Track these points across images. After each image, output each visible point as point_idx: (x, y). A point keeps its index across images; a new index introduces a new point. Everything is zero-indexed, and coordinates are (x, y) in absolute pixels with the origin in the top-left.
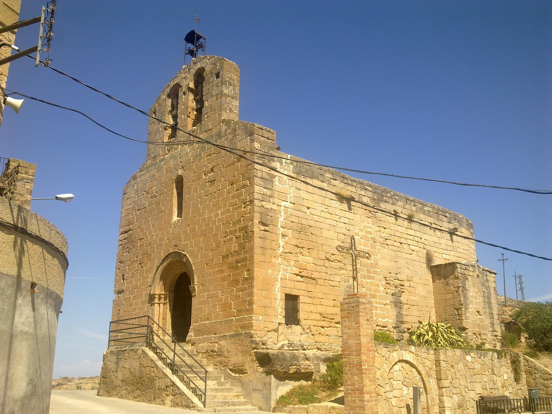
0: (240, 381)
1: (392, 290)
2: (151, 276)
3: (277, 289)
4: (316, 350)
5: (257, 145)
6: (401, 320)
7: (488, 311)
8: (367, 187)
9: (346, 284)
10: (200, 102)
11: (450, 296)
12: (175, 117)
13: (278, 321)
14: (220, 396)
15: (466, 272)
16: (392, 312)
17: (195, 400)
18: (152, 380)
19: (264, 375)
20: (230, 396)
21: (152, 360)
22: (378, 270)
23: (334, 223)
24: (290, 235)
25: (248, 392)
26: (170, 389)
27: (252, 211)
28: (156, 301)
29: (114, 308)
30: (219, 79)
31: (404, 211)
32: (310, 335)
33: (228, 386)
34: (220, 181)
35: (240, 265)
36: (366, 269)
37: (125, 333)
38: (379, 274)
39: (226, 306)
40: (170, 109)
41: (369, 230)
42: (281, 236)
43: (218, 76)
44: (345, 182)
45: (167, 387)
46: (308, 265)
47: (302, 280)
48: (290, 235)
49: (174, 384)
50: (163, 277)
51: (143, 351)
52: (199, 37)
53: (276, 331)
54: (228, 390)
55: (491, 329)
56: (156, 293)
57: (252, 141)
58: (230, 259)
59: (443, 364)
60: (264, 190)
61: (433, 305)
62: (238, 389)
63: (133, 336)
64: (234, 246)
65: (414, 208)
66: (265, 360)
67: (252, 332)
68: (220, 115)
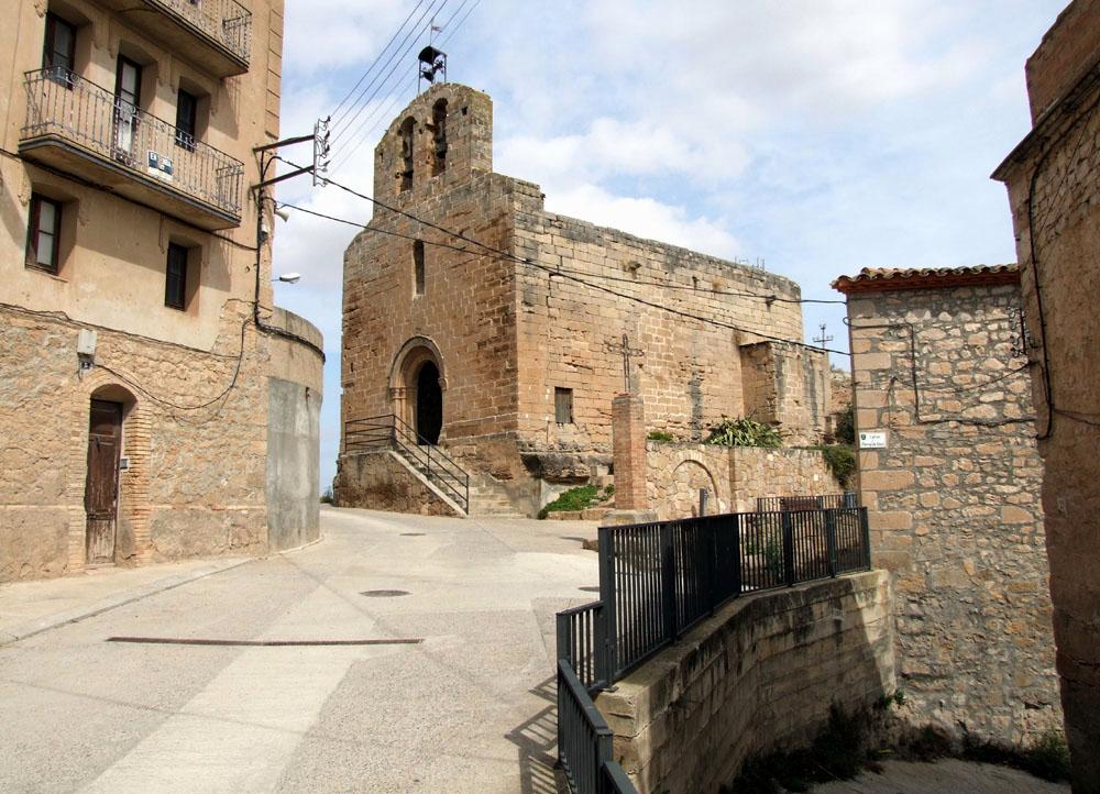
0: (504, 486)
1: (688, 377)
2: (389, 365)
5: (517, 205)
7: (809, 400)
10: (440, 140)
11: (762, 383)
12: (409, 160)
14: (484, 504)
15: (783, 353)
16: (689, 405)
17: (456, 507)
18: (404, 487)
19: (532, 479)
20: (494, 504)
21: (402, 466)
25: (514, 497)
26: (427, 497)
27: (513, 288)
28: (397, 396)
29: (343, 405)
30: (467, 117)
31: (707, 277)
32: (585, 434)
33: (491, 492)
35: (499, 353)
37: (359, 439)
39: (485, 403)
40: (401, 150)
43: (465, 111)
45: (423, 494)
47: (576, 369)
49: (430, 491)
50: (405, 367)
51: (391, 456)
53: (546, 430)
54: (492, 497)
55: (813, 423)
56: (740, 510)
57: (511, 200)
58: (490, 347)
59: (738, 464)
61: (741, 395)
62: (502, 497)
63: (371, 438)
64: (492, 331)
65: (719, 273)
66: (534, 465)
67: (517, 432)
68: (469, 164)
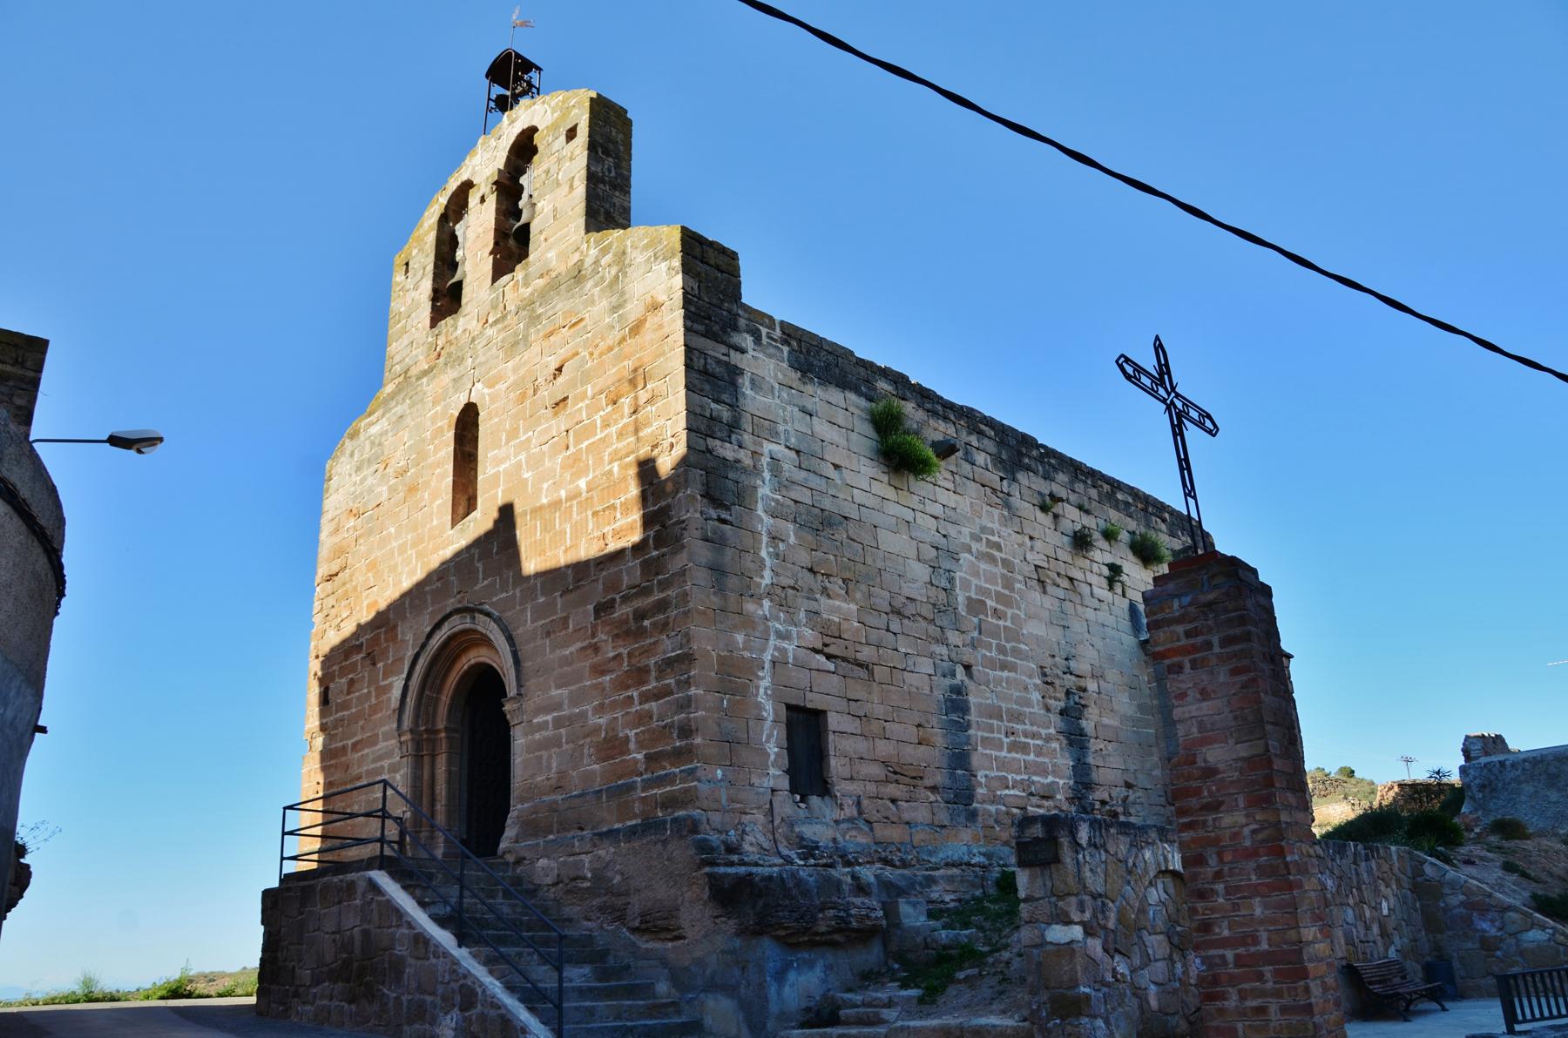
3: (762, 691)
4: (878, 865)
6: (1085, 780)
8: (983, 427)
9: (948, 681)
13: (769, 783)
22: (1023, 646)
23: (909, 515)
24: (792, 540)
34: (583, 396)
36: (994, 642)
38: (1026, 658)
41: (995, 539)
42: (765, 539)
44: (929, 406)
46: (845, 625)
47: (831, 667)
48: (792, 540)
52: (528, 66)
58: (623, 611)
60: (713, 405)
65: (1093, 493)
